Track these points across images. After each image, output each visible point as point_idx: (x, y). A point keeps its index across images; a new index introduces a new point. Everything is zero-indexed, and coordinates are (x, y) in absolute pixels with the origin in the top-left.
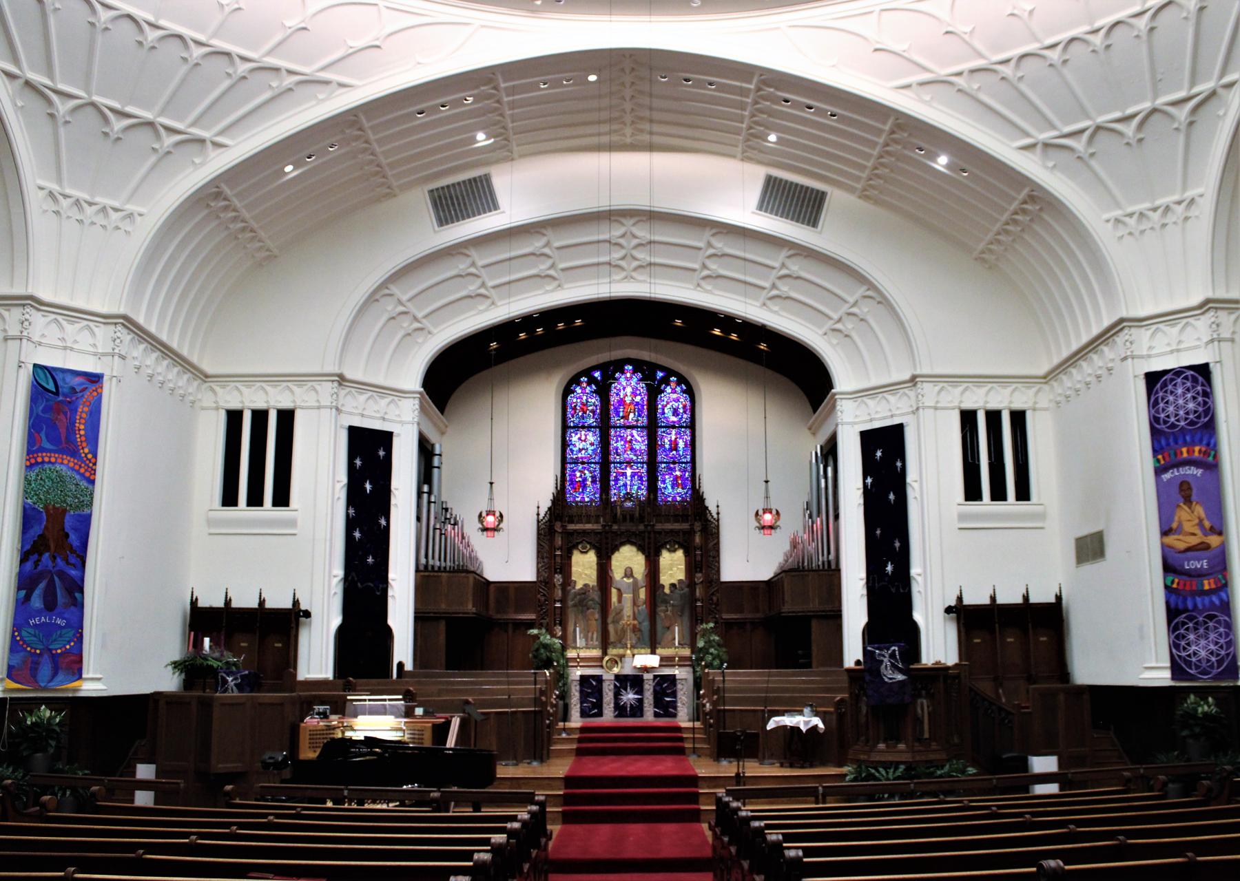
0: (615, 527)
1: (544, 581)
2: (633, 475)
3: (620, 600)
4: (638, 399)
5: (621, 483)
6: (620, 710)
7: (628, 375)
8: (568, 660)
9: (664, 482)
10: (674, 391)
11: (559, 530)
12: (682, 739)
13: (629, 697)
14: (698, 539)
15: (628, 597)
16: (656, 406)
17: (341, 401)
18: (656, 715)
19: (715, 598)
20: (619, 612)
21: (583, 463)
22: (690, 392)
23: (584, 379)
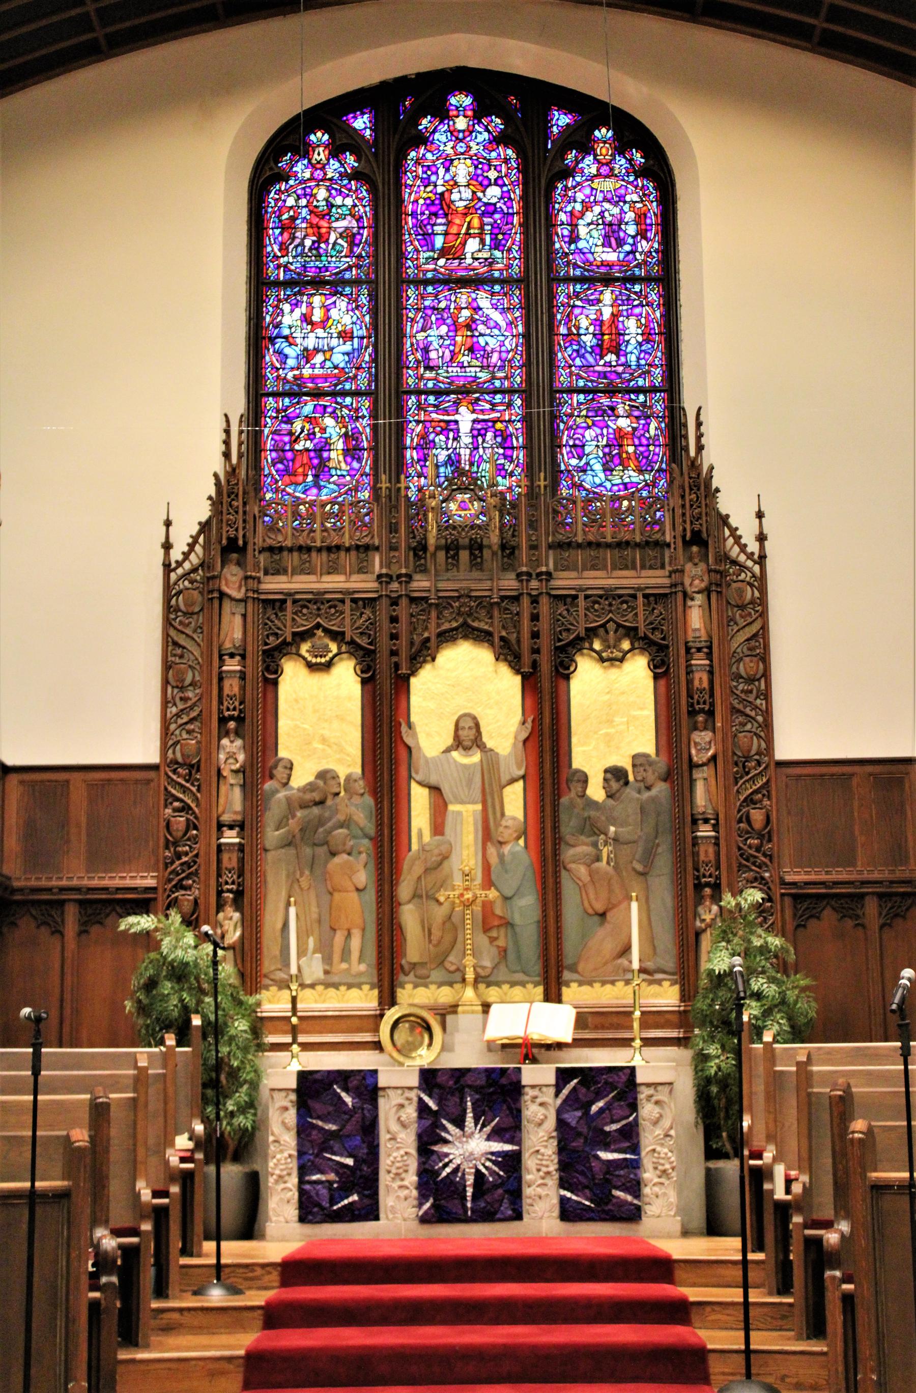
0: (421, 583)
1: (184, 767)
3: (438, 828)
4: (493, 193)
6: (441, 1196)
7: (461, 123)
8: (258, 1026)
9: (579, 449)
11: (235, 601)
12: (679, 1311)
13: (471, 1148)
14: (696, 619)
15: (465, 814)
16: (551, 223)
18: (568, 1213)
19: (757, 816)
20: (439, 862)
21: (317, 394)
22: (658, 172)
23: (319, 137)
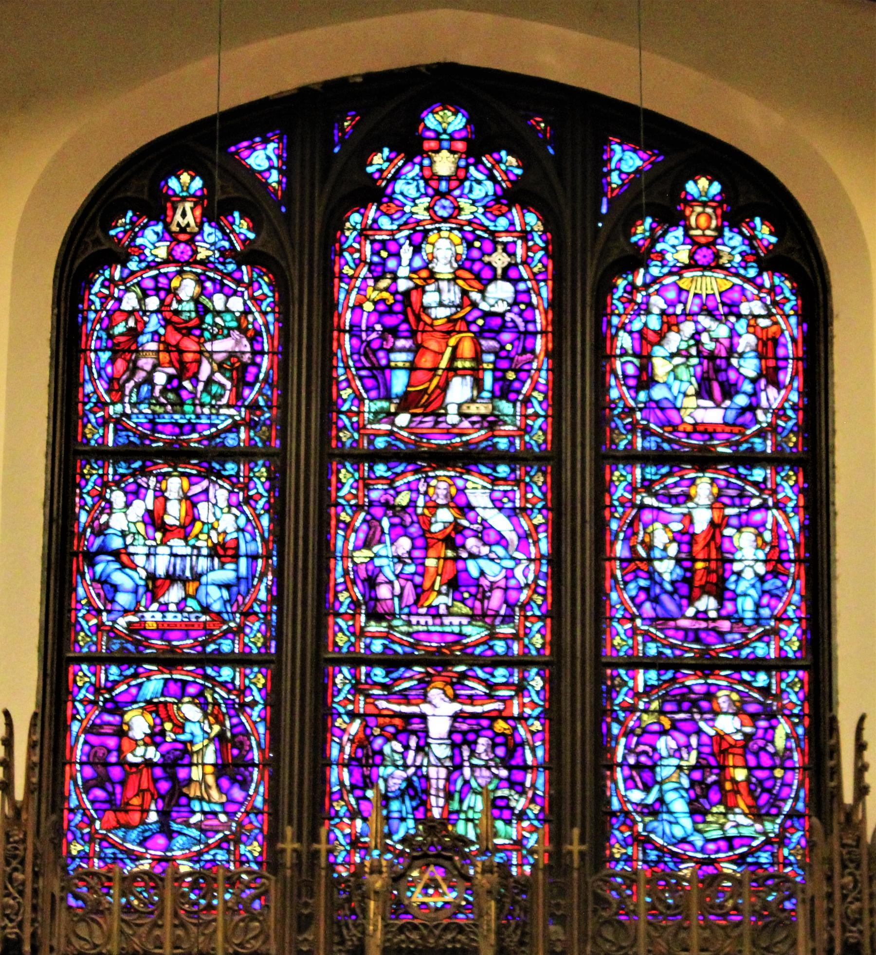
2: (461, 738)
4: (500, 294)
5: (392, 776)
7: (444, 164)
9: (645, 773)
10: (705, 258)
16: (603, 352)
17: (118, 607)
21: (169, 661)
22: (800, 262)
23: (186, 183)
